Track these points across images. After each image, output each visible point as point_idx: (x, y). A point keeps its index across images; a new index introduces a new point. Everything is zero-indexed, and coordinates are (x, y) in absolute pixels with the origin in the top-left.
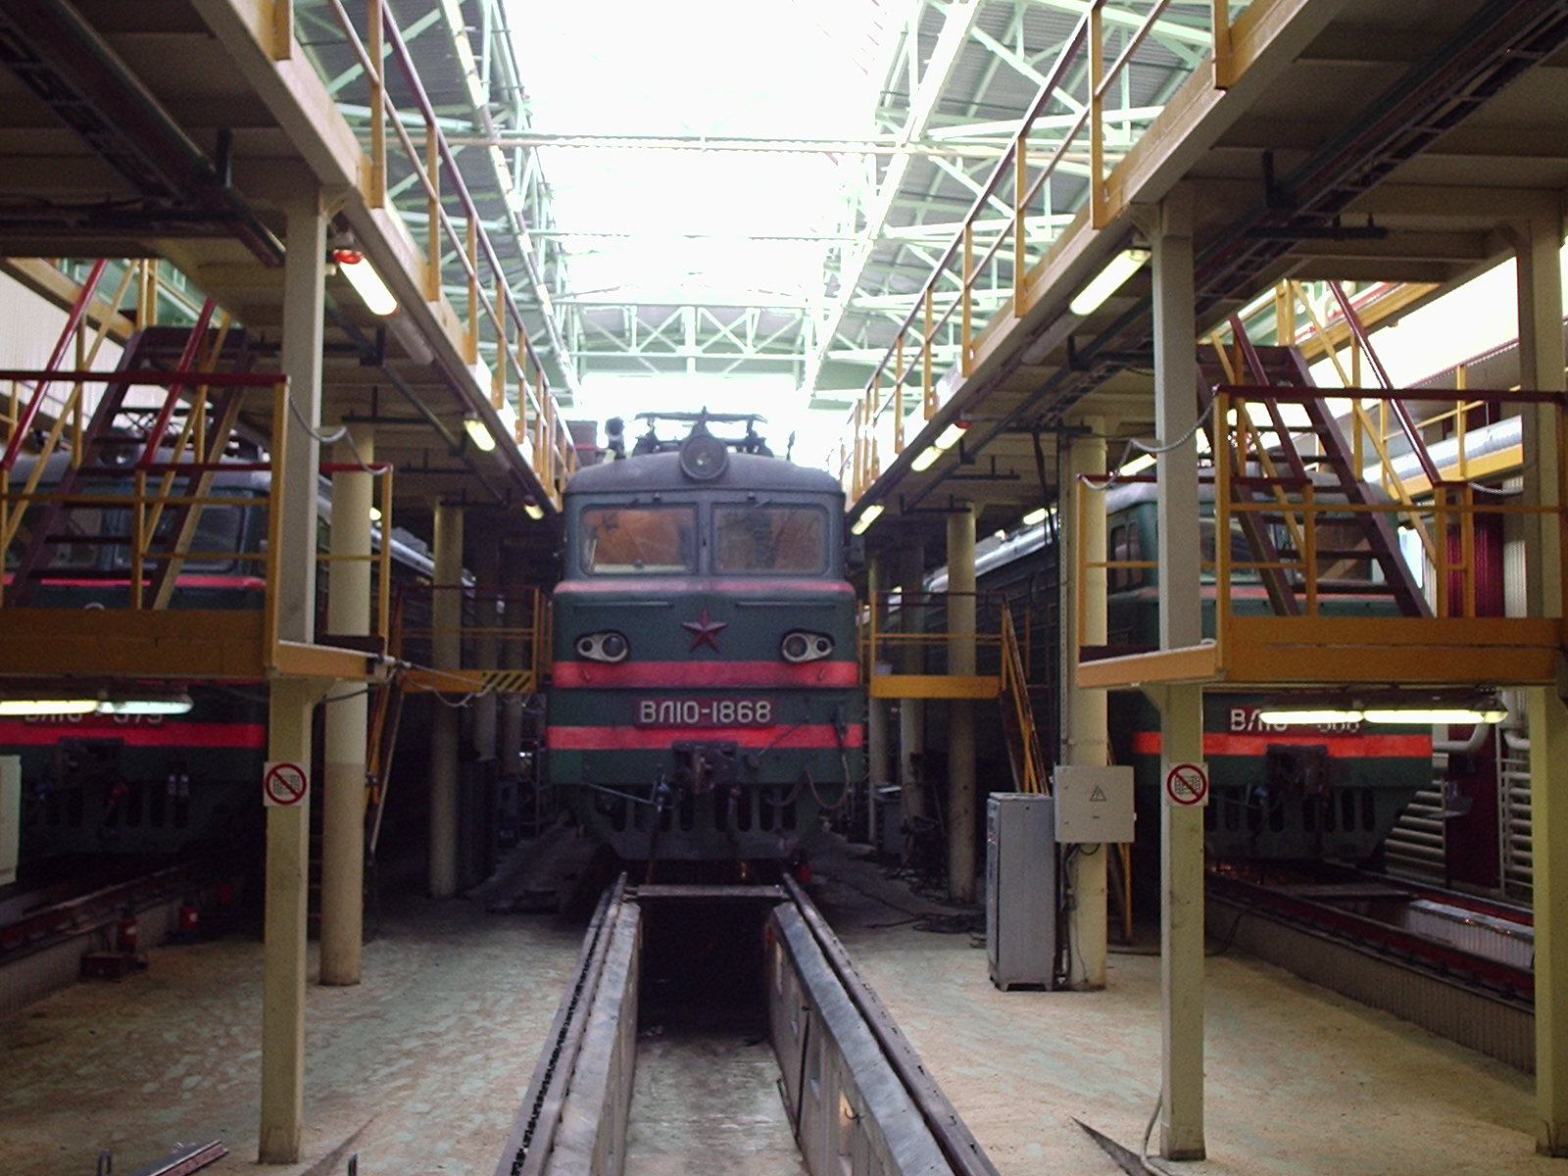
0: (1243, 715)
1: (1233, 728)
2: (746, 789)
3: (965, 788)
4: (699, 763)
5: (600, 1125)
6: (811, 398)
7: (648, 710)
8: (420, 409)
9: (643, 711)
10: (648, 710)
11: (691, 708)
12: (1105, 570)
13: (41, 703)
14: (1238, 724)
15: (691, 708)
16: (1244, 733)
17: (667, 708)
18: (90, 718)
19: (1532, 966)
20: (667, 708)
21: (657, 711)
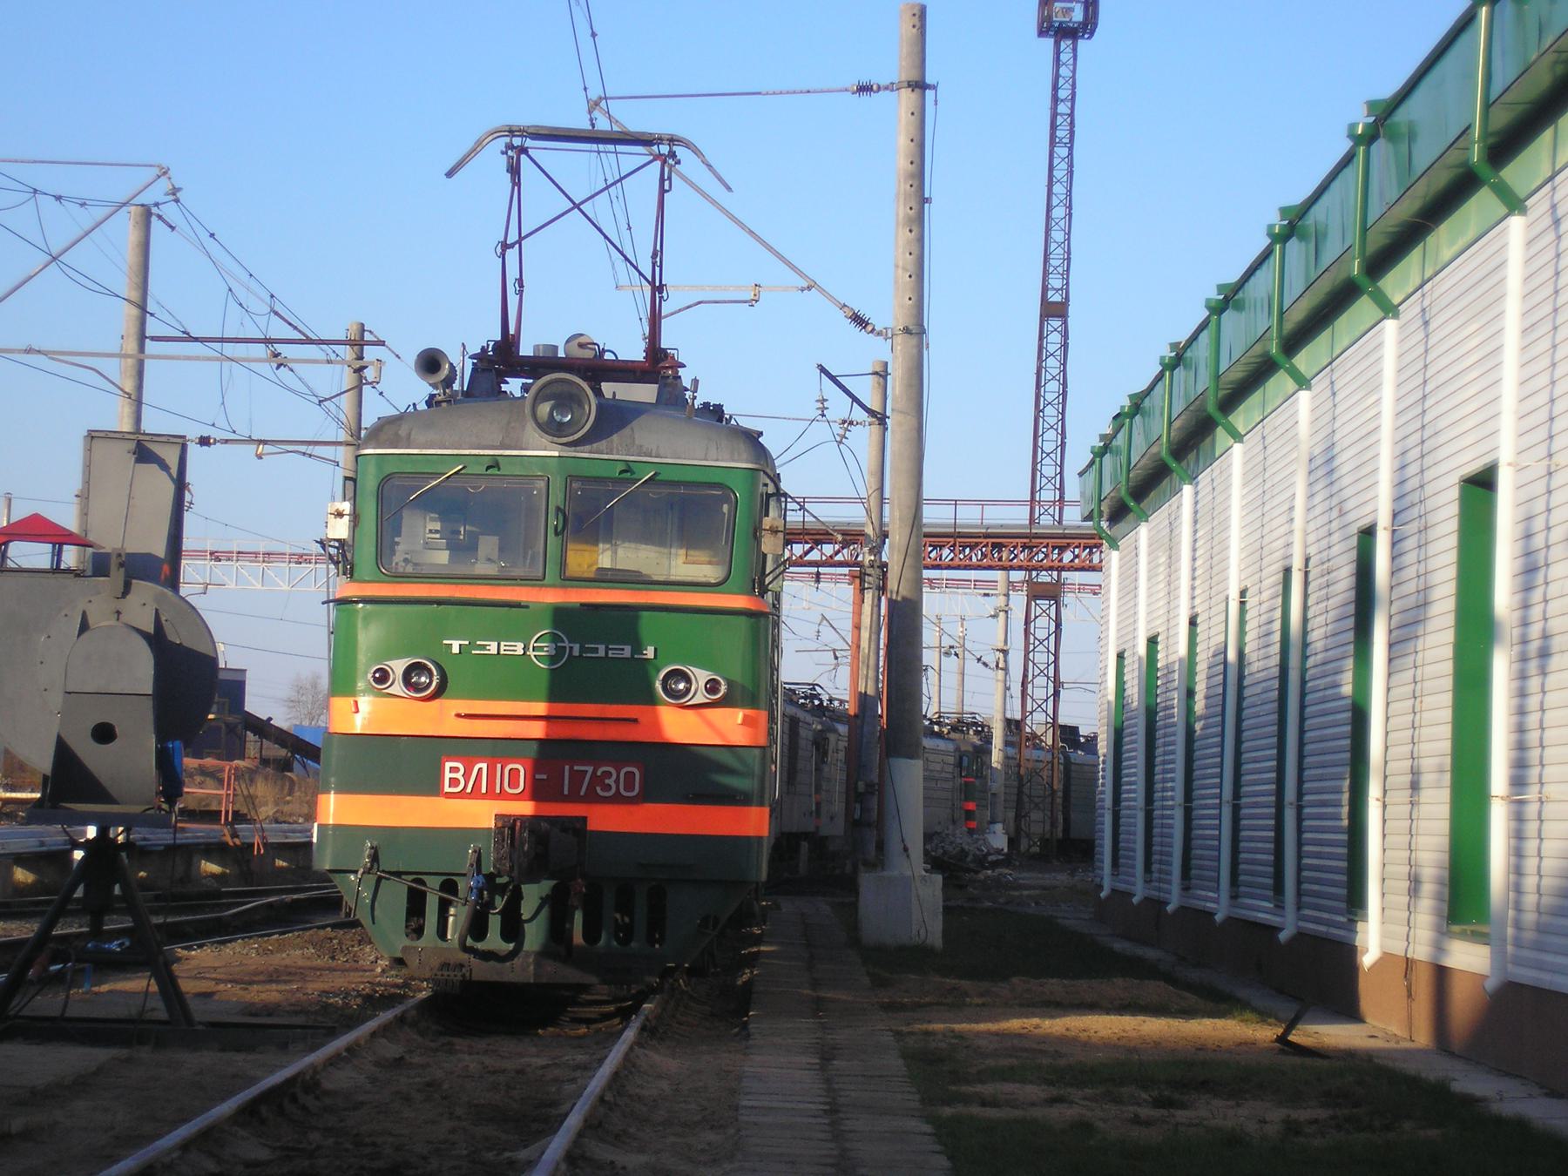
0: (462, 771)
1: (447, 789)
2: (1006, 787)
3: (938, 746)
4: (1101, 842)
5: (1152, 831)
6: (193, 432)
7: (454, 775)
8: (769, 574)
9: (448, 775)
10: (454, 775)
11: (630, 775)
12: (1033, 751)
13: (89, 805)
14: (454, 782)
15: (630, 775)
16: (462, 795)
17: (480, 769)
18: (51, 783)
19: (1531, 208)
20: (480, 769)
21: (467, 776)
